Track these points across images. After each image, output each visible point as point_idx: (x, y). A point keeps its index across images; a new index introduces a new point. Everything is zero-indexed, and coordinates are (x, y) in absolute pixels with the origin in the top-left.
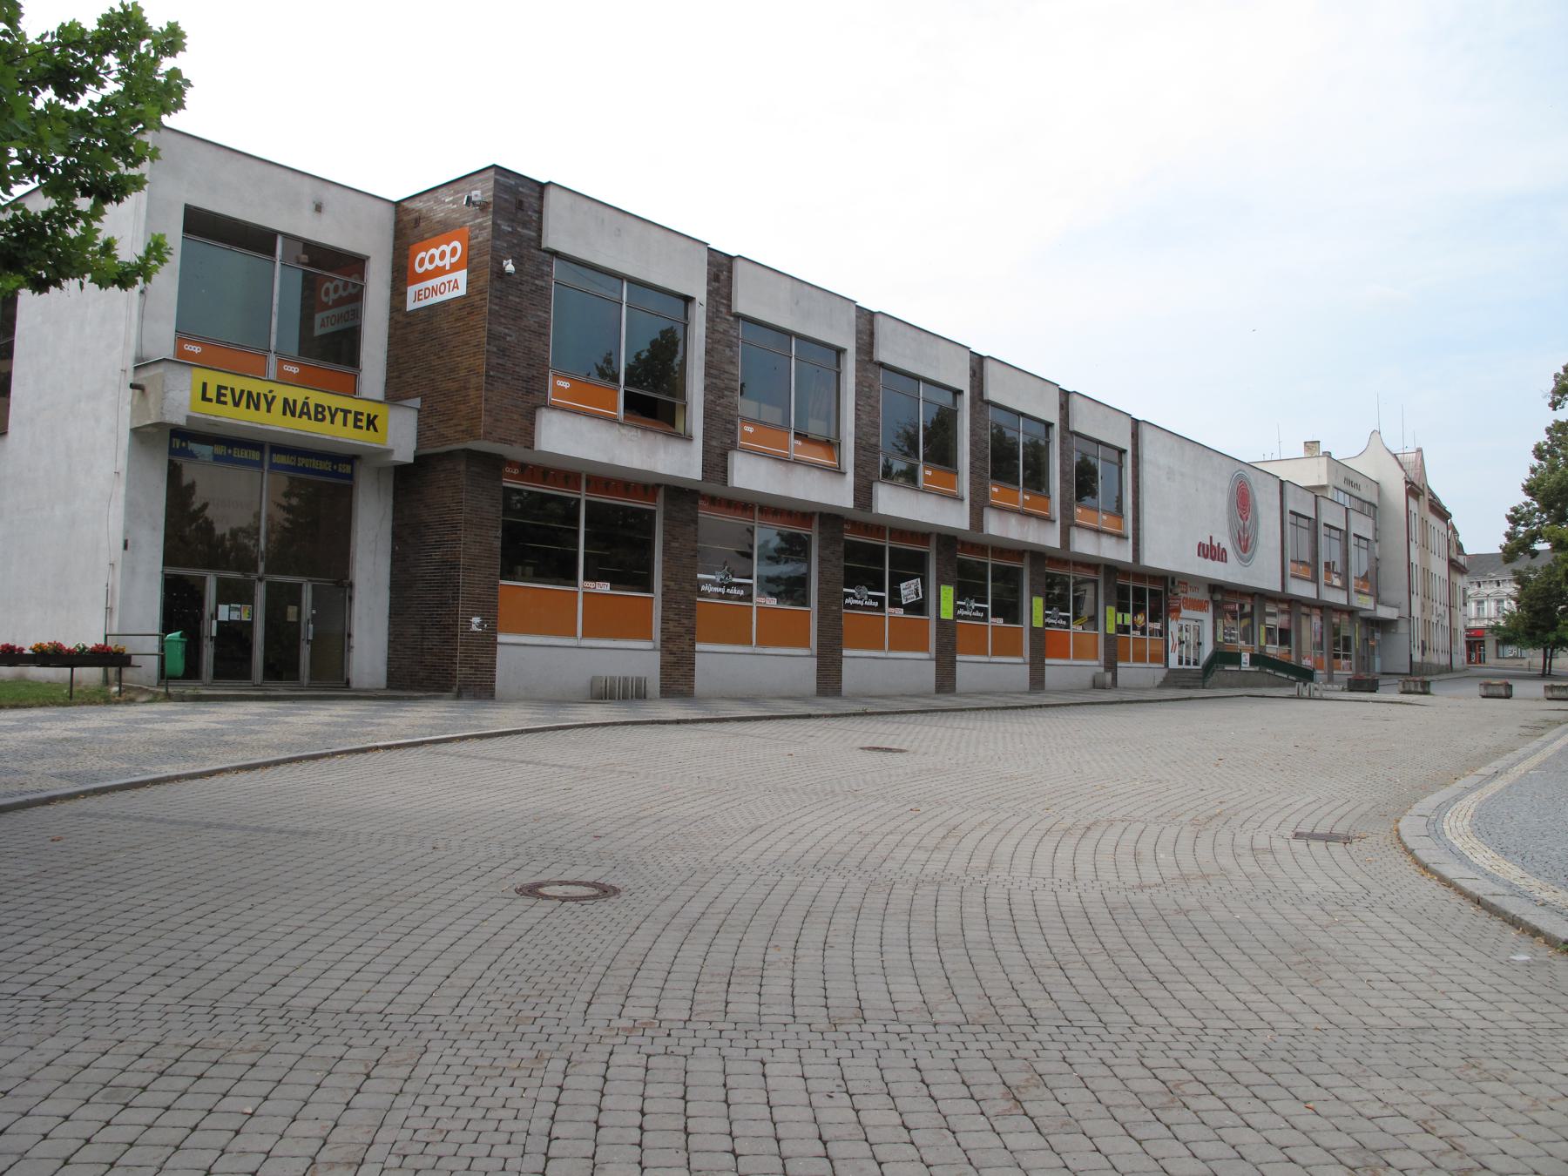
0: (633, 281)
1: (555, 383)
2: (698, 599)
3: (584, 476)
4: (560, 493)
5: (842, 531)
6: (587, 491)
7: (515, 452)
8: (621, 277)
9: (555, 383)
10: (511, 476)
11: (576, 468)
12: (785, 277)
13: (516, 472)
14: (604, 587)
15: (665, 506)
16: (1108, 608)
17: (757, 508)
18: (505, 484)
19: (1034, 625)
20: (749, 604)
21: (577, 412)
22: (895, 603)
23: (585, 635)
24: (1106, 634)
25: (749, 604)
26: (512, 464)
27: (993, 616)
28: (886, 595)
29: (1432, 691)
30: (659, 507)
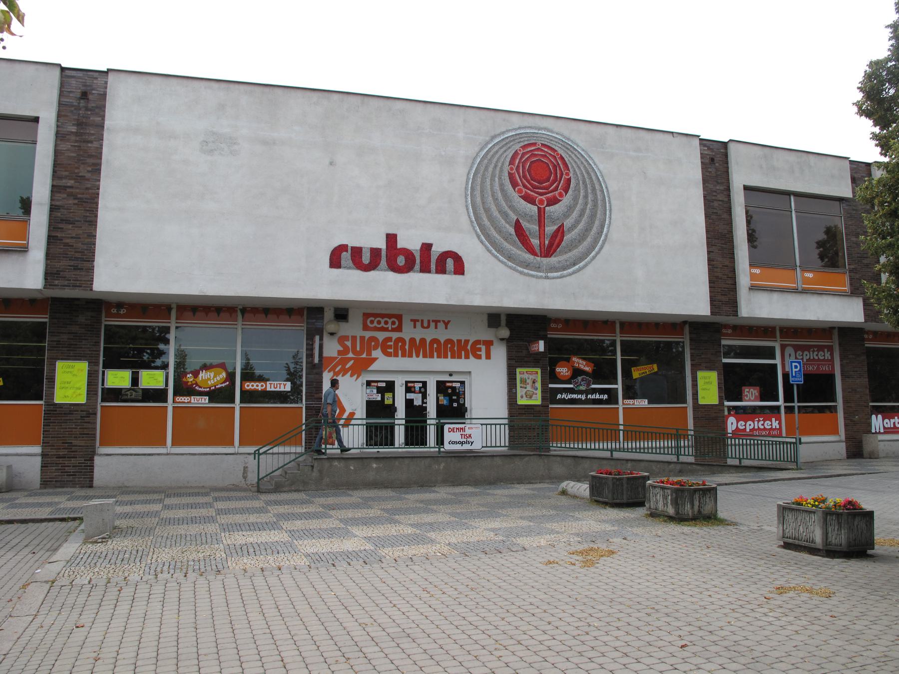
0: (798, 195)
1: (803, 276)
2: (551, 406)
3: (174, 306)
4: (628, 339)
5: (864, 340)
6: (781, 338)
7: (731, 320)
8: (788, 193)
9: (803, 276)
10: (869, 340)
11: (611, 318)
12: (780, 150)
13: (730, 331)
14: (643, 403)
15: (839, 340)
16: (700, 374)
17: (618, 326)
18: (866, 345)
19: (701, 402)
20: (616, 406)
21: (771, 290)
22: (630, 393)
23: (241, 444)
24: (697, 406)
25: (616, 406)
26: (726, 326)
27: (624, 398)
28: (619, 386)
29: (721, 514)
30: (686, 339)
